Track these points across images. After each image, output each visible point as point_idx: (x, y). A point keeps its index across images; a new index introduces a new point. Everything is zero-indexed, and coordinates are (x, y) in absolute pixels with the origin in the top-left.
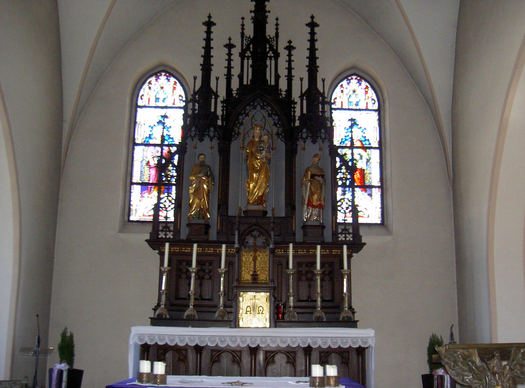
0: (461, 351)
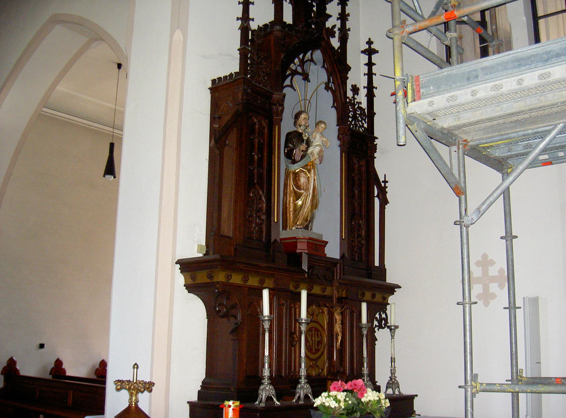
0: (330, 84)
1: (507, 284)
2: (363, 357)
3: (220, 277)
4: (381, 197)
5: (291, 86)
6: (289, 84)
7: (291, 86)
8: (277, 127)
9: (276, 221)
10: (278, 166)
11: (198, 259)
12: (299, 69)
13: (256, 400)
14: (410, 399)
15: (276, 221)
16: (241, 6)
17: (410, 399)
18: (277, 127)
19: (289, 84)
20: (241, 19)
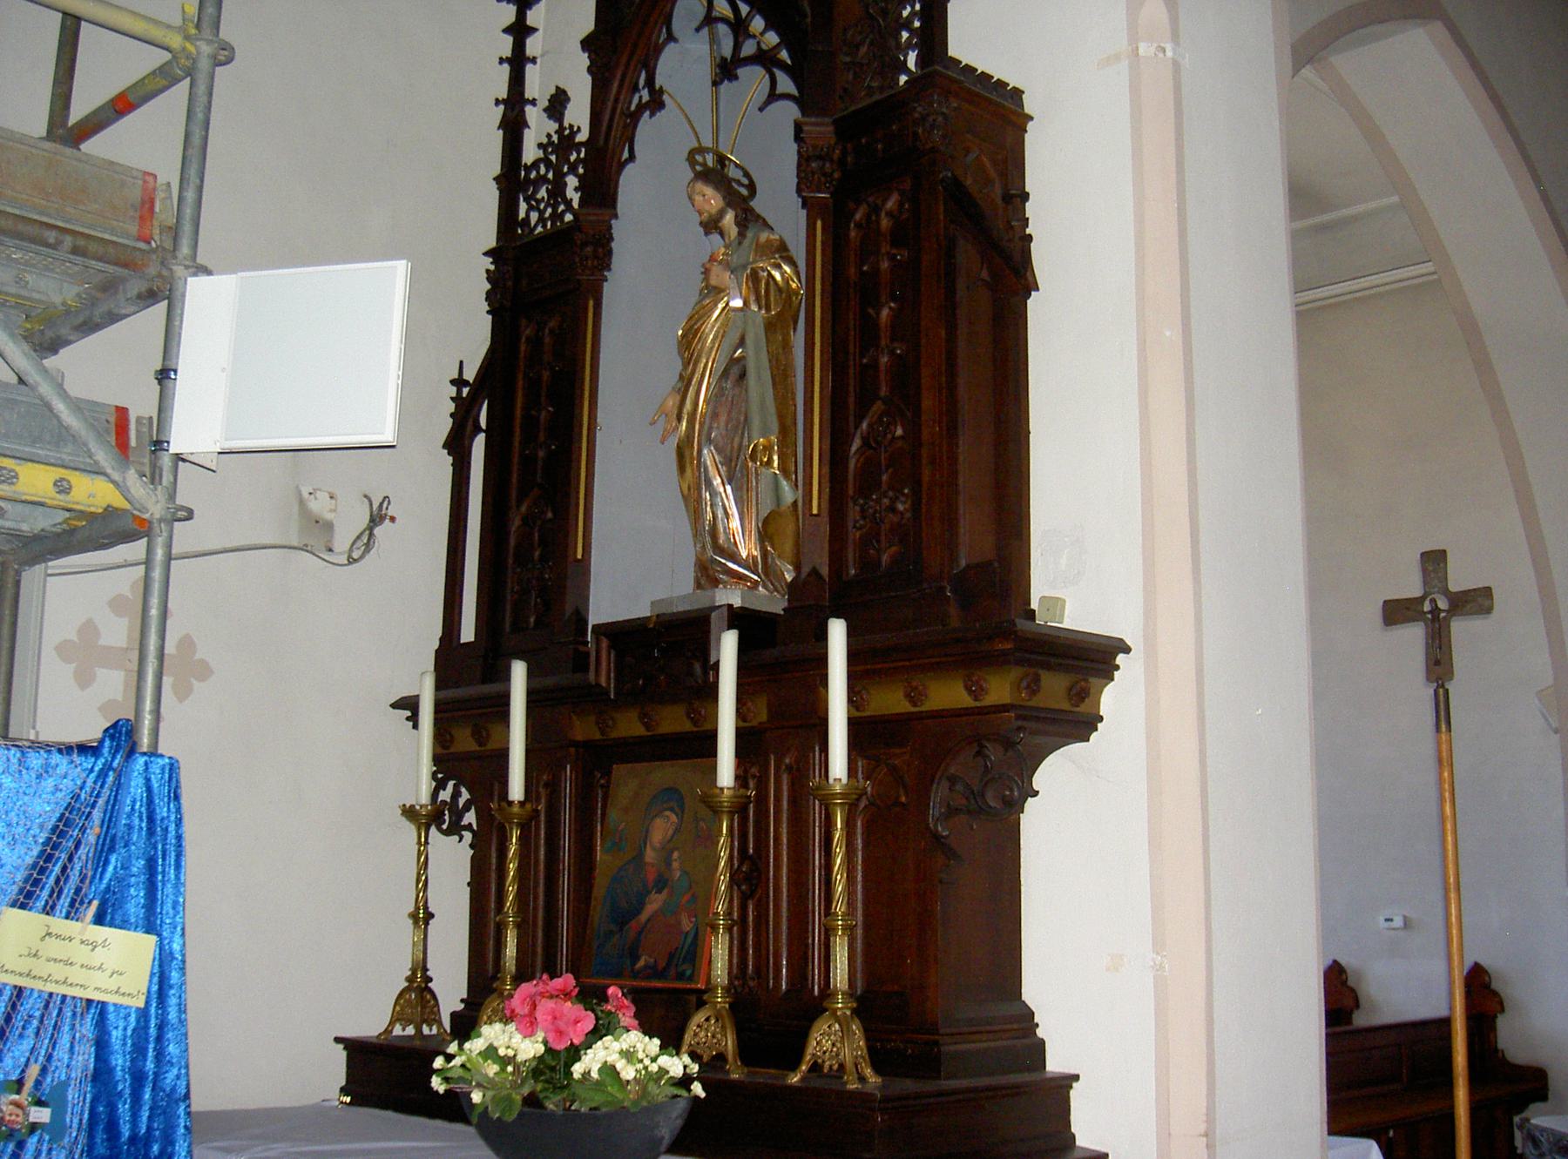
1: (170, 648)
2: (518, 926)
3: (1000, 689)
4: (470, 422)
5: (773, 96)
6: (780, 89)
7: (773, 96)
8: (591, 303)
9: (815, 511)
10: (813, 344)
11: (1080, 637)
12: (749, 49)
13: (794, 1067)
14: (357, 1050)
15: (815, 511)
16: (506, 67)
17: (357, 1050)
18: (591, 303)
19: (780, 89)
20: (504, 101)
